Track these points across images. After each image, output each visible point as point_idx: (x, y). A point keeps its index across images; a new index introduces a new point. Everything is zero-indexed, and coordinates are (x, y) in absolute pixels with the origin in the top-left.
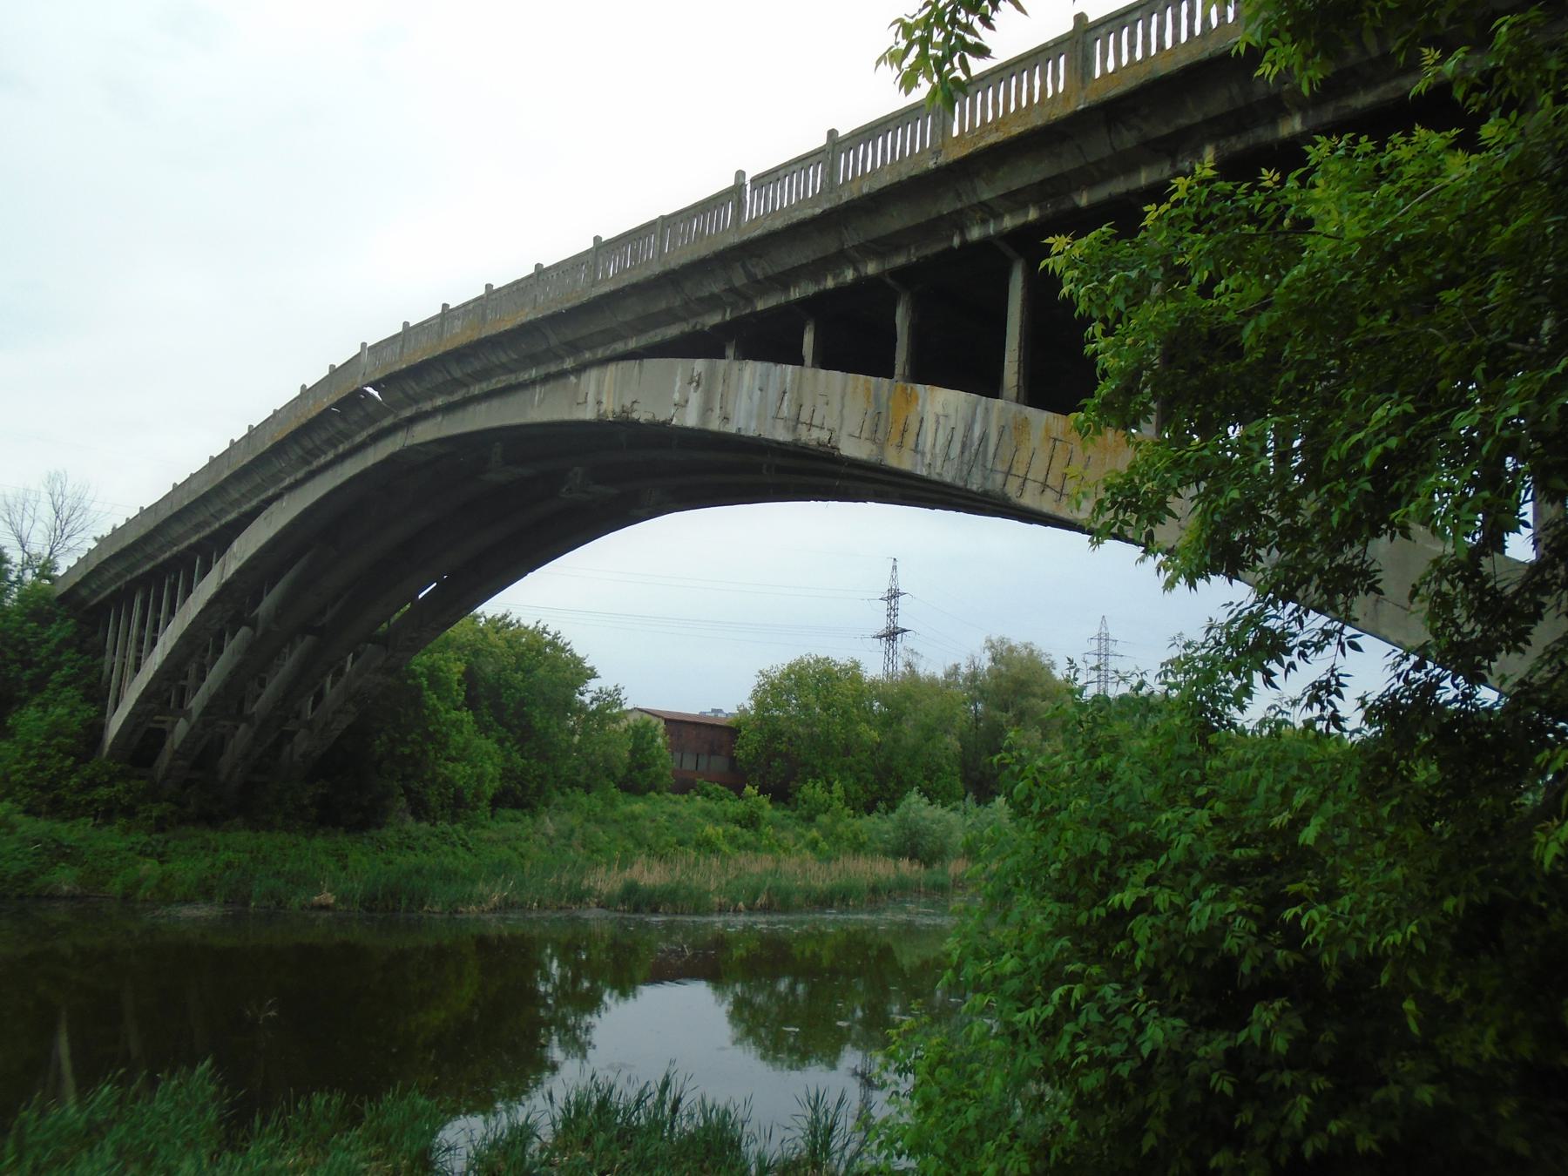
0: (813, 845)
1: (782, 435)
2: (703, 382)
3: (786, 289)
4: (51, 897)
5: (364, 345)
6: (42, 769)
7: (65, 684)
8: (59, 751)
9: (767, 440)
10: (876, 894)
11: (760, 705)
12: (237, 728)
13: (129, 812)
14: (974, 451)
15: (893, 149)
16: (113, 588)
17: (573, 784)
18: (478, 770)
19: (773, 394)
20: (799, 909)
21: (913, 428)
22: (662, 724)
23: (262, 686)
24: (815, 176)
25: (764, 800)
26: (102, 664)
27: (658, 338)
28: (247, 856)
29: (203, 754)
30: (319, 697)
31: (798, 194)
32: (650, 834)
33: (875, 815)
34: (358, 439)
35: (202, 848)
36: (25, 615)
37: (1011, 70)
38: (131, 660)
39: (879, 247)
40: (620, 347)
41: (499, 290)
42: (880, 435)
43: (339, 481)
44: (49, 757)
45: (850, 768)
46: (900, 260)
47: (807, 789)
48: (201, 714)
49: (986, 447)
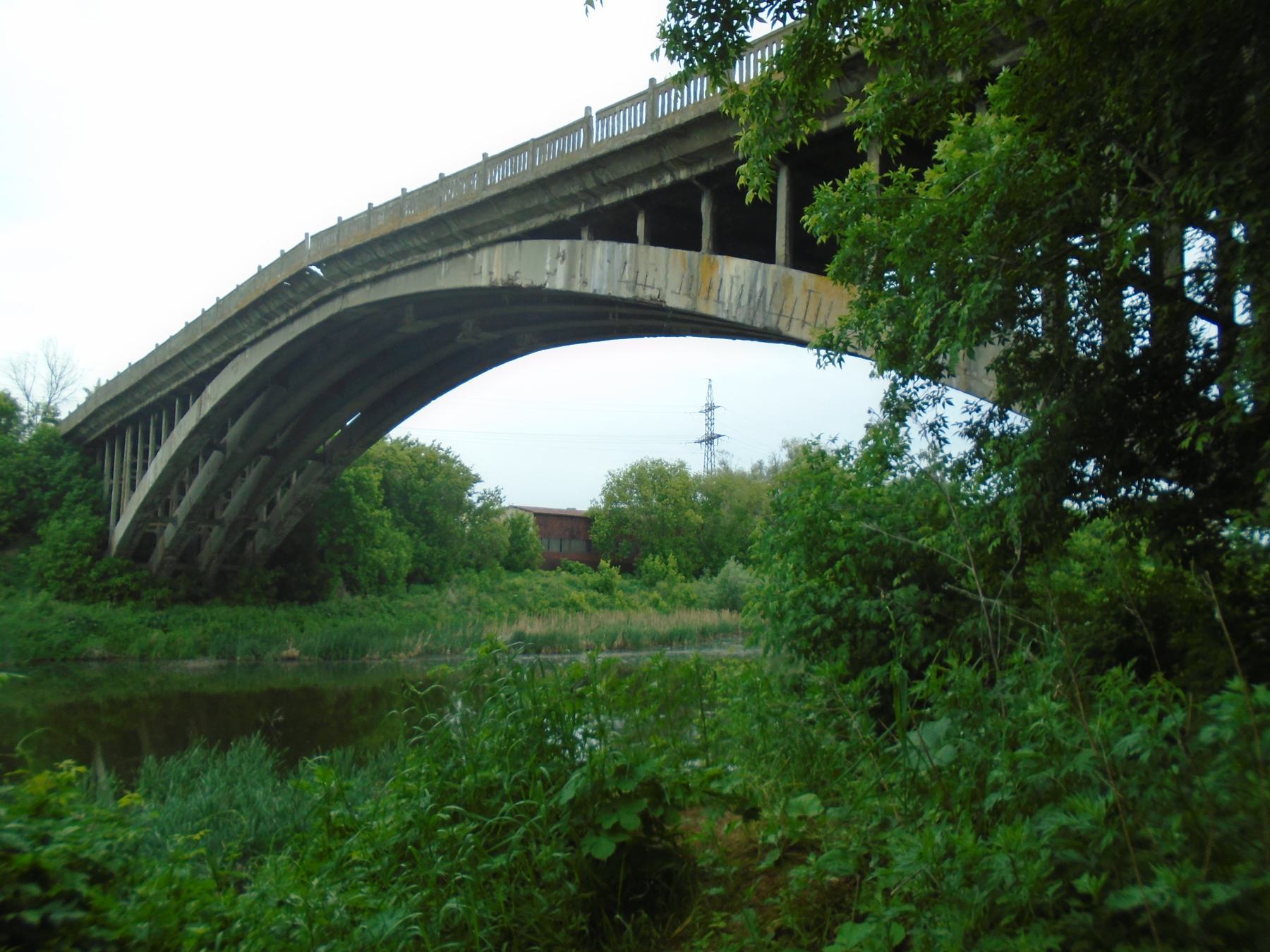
0: (655, 604)
1: (625, 293)
2: (567, 256)
3: (623, 189)
4: (87, 659)
5: (307, 235)
6: (68, 566)
7: (76, 502)
8: (79, 552)
9: (614, 297)
10: (705, 635)
11: (609, 499)
12: (210, 530)
13: (136, 596)
14: (757, 301)
15: (695, 93)
16: (108, 426)
17: (466, 565)
18: (396, 556)
19: (617, 264)
20: (647, 647)
21: (716, 286)
22: (533, 517)
23: (229, 496)
24: (641, 111)
25: (615, 570)
26: (103, 486)
27: (532, 226)
28: (229, 625)
29: (187, 552)
30: (271, 506)
31: (630, 124)
32: (529, 600)
33: (702, 579)
34: (305, 304)
35: (195, 620)
36: (40, 450)
37: (773, 39)
38: (127, 481)
39: (689, 160)
40: (504, 232)
41: (412, 192)
42: (693, 291)
43: (290, 338)
44: (71, 556)
45: (681, 545)
46: (702, 169)
47: (648, 562)
48: (185, 520)
49: (765, 298)
